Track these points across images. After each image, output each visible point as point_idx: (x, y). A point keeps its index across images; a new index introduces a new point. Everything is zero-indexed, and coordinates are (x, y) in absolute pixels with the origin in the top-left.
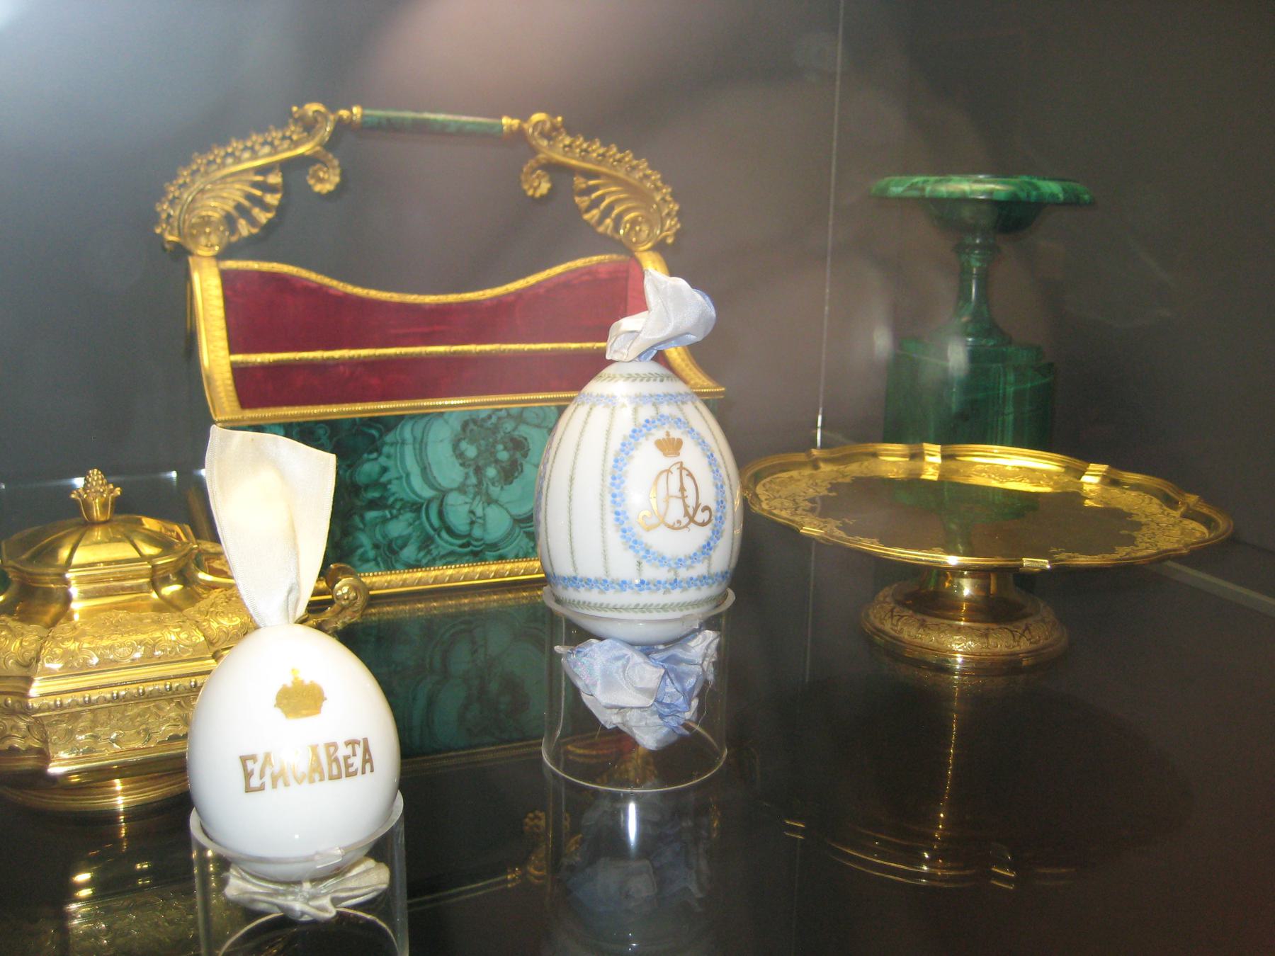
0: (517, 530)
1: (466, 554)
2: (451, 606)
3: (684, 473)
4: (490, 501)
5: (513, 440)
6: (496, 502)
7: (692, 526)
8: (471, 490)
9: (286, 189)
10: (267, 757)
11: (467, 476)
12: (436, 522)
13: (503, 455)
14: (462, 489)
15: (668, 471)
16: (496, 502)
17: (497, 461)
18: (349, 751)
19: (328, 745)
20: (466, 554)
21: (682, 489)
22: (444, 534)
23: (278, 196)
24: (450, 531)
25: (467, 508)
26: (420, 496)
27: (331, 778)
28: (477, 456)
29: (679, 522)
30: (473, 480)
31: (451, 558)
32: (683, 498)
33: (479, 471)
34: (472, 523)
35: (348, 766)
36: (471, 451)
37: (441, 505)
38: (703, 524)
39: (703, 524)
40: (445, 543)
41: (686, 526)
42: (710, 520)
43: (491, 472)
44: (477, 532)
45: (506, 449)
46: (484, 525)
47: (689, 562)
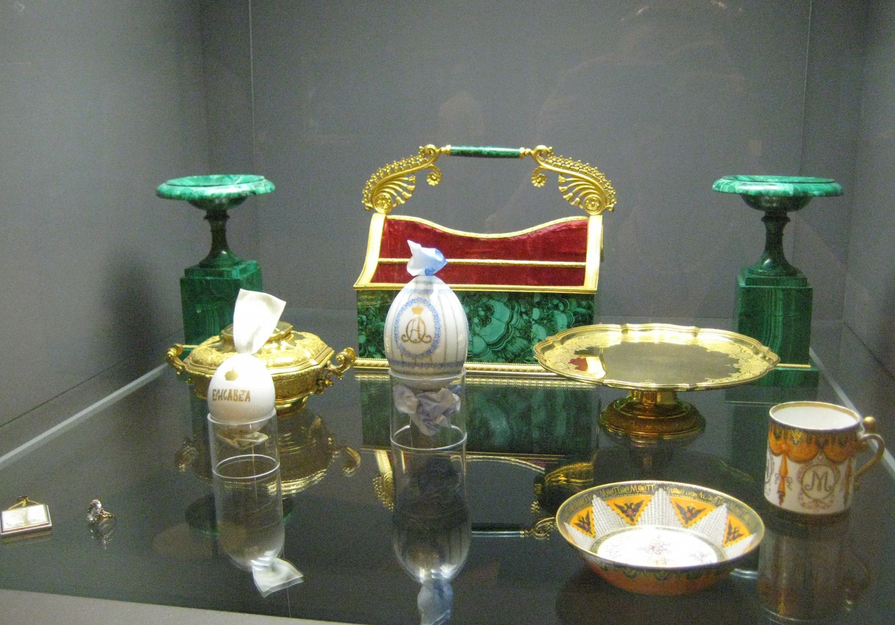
5: (486, 306)
6: (478, 335)
13: (482, 313)
16: (478, 335)
17: (478, 316)
21: (418, 328)
23: (413, 187)
32: (418, 331)
38: (426, 342)
39: (426, 342)
43: (476, 320)
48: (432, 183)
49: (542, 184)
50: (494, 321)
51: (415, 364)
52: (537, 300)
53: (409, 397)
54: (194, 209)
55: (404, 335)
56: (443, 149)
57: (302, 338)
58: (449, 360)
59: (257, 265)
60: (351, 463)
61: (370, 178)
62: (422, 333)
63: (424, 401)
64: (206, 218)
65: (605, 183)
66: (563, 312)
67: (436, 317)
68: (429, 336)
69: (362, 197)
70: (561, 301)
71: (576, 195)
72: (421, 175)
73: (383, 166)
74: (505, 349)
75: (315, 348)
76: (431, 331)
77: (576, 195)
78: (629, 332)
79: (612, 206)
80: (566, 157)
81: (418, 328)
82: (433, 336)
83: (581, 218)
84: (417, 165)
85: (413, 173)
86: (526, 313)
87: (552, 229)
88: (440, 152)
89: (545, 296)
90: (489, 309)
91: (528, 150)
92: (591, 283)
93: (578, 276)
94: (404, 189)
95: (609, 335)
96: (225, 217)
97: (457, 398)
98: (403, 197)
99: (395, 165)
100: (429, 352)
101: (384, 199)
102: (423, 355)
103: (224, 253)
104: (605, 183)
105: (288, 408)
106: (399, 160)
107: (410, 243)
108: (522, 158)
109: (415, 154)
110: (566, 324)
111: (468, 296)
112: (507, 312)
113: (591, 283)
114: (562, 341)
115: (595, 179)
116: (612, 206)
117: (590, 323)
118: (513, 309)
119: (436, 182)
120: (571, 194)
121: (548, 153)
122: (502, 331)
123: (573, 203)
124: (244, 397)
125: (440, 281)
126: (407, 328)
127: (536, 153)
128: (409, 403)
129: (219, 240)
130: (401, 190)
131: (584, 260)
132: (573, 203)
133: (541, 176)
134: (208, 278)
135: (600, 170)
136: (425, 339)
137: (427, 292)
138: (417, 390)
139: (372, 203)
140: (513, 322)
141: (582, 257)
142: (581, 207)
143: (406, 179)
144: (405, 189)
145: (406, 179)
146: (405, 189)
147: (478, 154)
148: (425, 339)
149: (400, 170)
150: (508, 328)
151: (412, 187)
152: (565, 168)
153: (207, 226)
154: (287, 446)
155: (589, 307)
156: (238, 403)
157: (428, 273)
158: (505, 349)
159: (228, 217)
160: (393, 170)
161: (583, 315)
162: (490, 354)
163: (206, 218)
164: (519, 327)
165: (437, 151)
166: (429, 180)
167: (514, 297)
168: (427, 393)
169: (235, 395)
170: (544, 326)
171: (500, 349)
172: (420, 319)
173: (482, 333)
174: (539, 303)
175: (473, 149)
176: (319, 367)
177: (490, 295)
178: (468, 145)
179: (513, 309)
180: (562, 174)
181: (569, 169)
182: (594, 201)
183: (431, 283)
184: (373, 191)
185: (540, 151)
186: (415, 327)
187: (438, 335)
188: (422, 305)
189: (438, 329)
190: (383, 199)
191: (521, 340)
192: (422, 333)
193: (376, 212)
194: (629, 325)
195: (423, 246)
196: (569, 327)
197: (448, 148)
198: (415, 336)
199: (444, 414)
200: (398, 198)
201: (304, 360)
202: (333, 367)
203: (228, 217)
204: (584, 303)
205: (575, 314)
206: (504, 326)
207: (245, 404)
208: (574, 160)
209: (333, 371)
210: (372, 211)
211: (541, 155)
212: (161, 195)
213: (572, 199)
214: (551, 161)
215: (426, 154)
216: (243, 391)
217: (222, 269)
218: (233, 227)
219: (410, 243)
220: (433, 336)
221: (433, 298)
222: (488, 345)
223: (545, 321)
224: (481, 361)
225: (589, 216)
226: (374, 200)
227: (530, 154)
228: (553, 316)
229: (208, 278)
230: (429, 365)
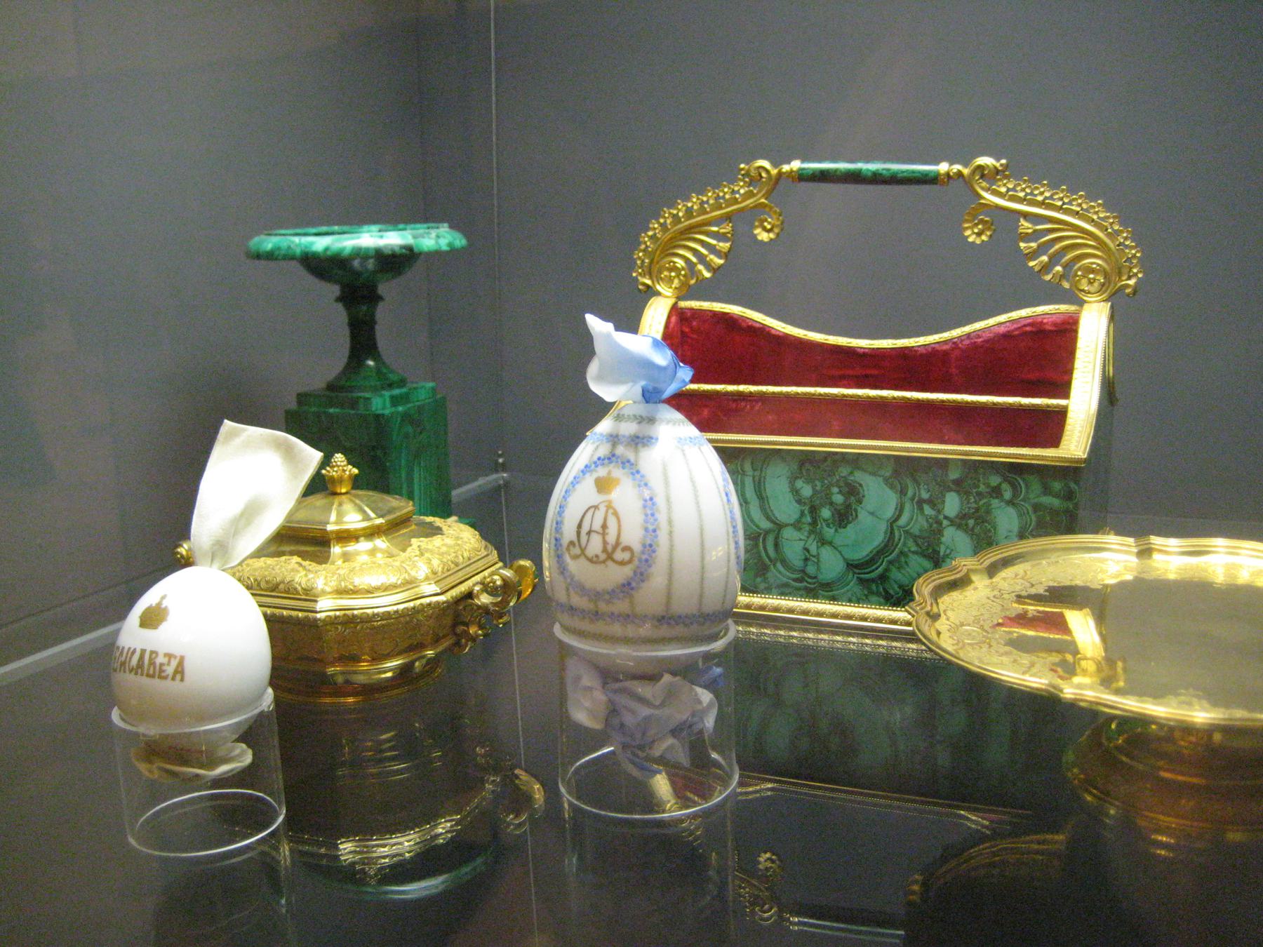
0: (851, 575)
1: (799, 589)
2: (883, 646)
3: (611, 511)
4: (823, 542)
5: (848, 484)
6: (830, 543)
7: (610, 563)
8: (807, 528)
9: (733, 238)
10: (182, 659)
11: (802, 514)
12: (772, 553)
13: (838, 499)
14: (797, 526)
15: (596, 507)
16: (830, 543)
17: (831, 504)
18: (165, 660)
19: (152, 652)
20: (799, 589)
21: (604, 526)
22: (779, 565)
23: (728, 245)
24: (784, 562)
25: (802, 543)
26: (757, 526)
27: (148, 675)
28: (812, 497)
29: (597, 556)
30: (808, 519)
31: (784, 590)
32: (604, 534)
33: (814, 510)
34: (806, 560)
35: (161, 671)
36: (807, 491)
37: (777, 538)
38: (622, 563)
39: (622, 563)
40: (778, 573)
41: (604, 562)
42: (630, 561)
43: (826, 513)
44: (811, 569)
45: (840, 492)
46: (818, 563)
47: (607, 597)
48: (764, 236)
49: (984, 238)
50: (862, 515)
51: (597, 616)
52: (954, 475)
53: (590, 689)
54: (311, 281)
55: (572, 543)
56: (786, 168)
57: (437, 531)
58: (679, 607)
59: (434, 389)
60: (520, 800)
61: (648, 229)
62: (611, 539)
63: (623, 700)
64: (339, 299)
65: (1118, 233)
66: (1011, 503)
67: (649, 504)
68: (627, 548)
69: (632, 265)
70: (1006, 479)
71: (1054, 259)
72: (743, 219)
73: (673, 205)
74: (883, 578)
75: (447, 558)
76: (633, 535)
77: (1054, 259)
78: (1156, 556)
79: (1132, 282)
80: (1035, 180)
81: (604, 526)
82: (637, 547)
83: (1063, 308)
84: (736, 201)
85: (728, 218)
86: (930, 502)
87: (1002, 329)
88: (780, 174)
89: (975, 467)
90: (853, 491)
91: (957, 167)
92: (1076, 443)
93: (1049, 427)
94: (705, 253)
95: (1109, 560)
96: (373, 298)
97: (706, 696)
98: (708, 266)
99: (694, 202)
100: (627, 588)
101: (674, 269)
102: (612, 593)
103: (371, 363)
104: (1118, 233)
105: (387, 679)
106: (702, 192)
107: (592, 320)
108: (943, 183)
109: (733, 181)
110: (1016, 529)
111: (811, 462)
112: (892, 499)
113: (1076, 443)
114: (992, 571)
115: (1097, 225)
116: (1132, 282)
117: (1070, 530)
118: (903, 492)
119: (772, 235)
120: (1045, 258)
121: (997, 172)
122: (878, 539)
123: (1048, 277)
124: (170, 670)
125: (678, 416)
126: (580, 526)
127: (973, 172)
128: (587, 704)
129: (363, 341)
130: (704, 251)
131: (1065, 394)
132: (1048, 277)
133: (981, 221)
134: (331, 410)
135: (1107, 207)
136: (619, 555)
137: (640, 441)
138: (608, 675)
139: (651, 278)
140: (902, 522)
141: (1061, 387)
142: (1066, 285)
143: (715, 229)
144: (712, 249)
145: (715, 229)
146: (712, 249)
147: (854, 178)
148: (619, 555)
149: (702, 211)
150: (892, 533)
151: (724, 246)
152: (1032, 203)
153: (340, 315)
154: (381, 761)
155: (1069, 496)
156: (156, 681)
157: (649, 396)
158: (883, 578)
159: (380, 298)
160: (689, 212)
161: (1054, 512)
162: (853, 586)
163: (339, 299)
164: (916, 531)
165: (774, 172)
166: (757, 231)
167: (906, 468)
168: (628, 684)
169: (152, 663)
170: (970, 531)
171: (873, 575)
172: (609, 506)
173: (838, 540)
174: (958, 483)
175: (843, 166)
176: (442, 598)
177: (856, 461)
178: (834, 160)
179: (903, 492)
180: (1026, 216)
181: (1042, 204)
182: (1093, 271)
183: (651, 420)
184: (654, 252)
185: (980, 167)
186: (597, 525)
187: (650, 548)
188: (618, 473)
189: (651, 531)
190: (671, 270)
191: (916, 557)
192: (611, 539)
193: (658, 294)
194: (1156, 541)
195: (617, 329)
196: (1022, 536)
197: (796, 165)
198: (595, 546)
199: (674, 732)
200: (700, 267)
201: (410, 583)
202: (485, 599)
203: (380, 298)
204: (1057, 486)
205: (1036, 507)
206: (883, 527)
207: (171, 687)
208: (1054, 186)
209: (485, 610)
210: (650, 292)
211: (982, 176)
212: (258, 256)
213: (1046, 268)
214: (1003, 190)
215: (754, 179)
216: (169, 656)
217: (355, 395)
218: (387, 320)
219: (592, 320)
220: (637, 547)
221: (651, 459)
222: (851, 566)
223: (971, 522)
224: (833, 599)
225: (1081, 303)
226: (655, 269)
227: (960, 174)
228: (988, 512)
229: (331, 410)
230: (627, 618)
